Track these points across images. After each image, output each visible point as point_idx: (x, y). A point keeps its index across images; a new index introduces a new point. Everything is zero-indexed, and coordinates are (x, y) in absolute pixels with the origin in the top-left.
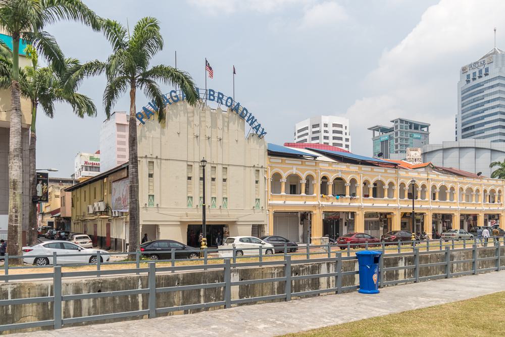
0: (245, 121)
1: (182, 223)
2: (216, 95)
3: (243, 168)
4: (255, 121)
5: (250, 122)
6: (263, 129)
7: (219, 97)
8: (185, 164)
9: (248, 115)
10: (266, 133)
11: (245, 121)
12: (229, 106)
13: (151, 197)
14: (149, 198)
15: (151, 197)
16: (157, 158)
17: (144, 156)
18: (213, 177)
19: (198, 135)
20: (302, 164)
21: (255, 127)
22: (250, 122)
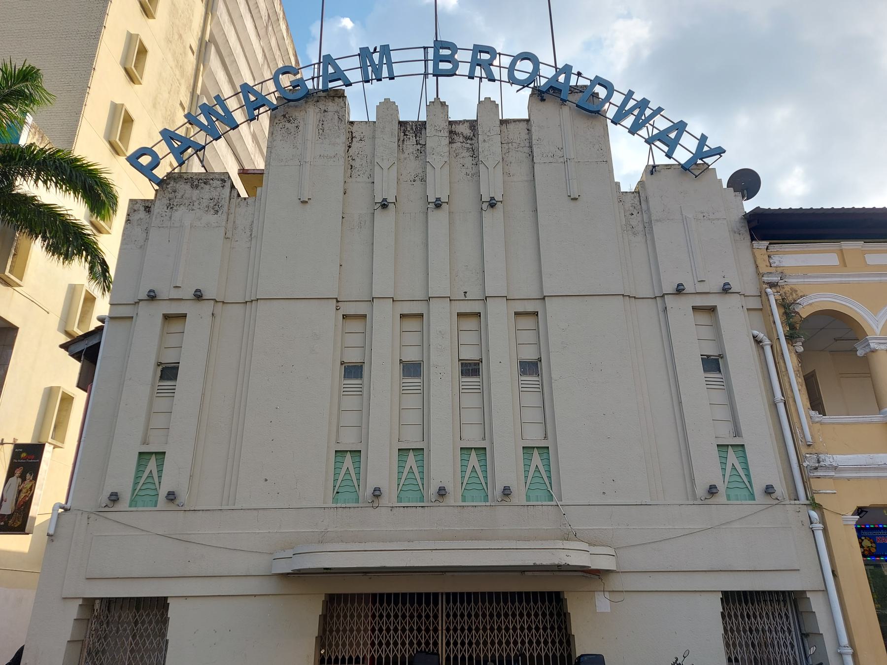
0: (609, 121)
1: (299, 578)
2: (464, 56)
3: (212, 302)
4: (652, 116)
5: (629, 121)
6: (703, 139)
7: (475, 63)
8: (328, 316)
9: (617, 99)
10: (720, 152)
11: (609, 121)
12: (524, 84)
13: (411, 459)
14: (464, 462)
15: (411, 459)
16: (198, 296)
17: (143, 295)
18: (169, 358)
19: (391, 199)
20: (844, 263)
21: (662, 137)
22: (629, 121)
